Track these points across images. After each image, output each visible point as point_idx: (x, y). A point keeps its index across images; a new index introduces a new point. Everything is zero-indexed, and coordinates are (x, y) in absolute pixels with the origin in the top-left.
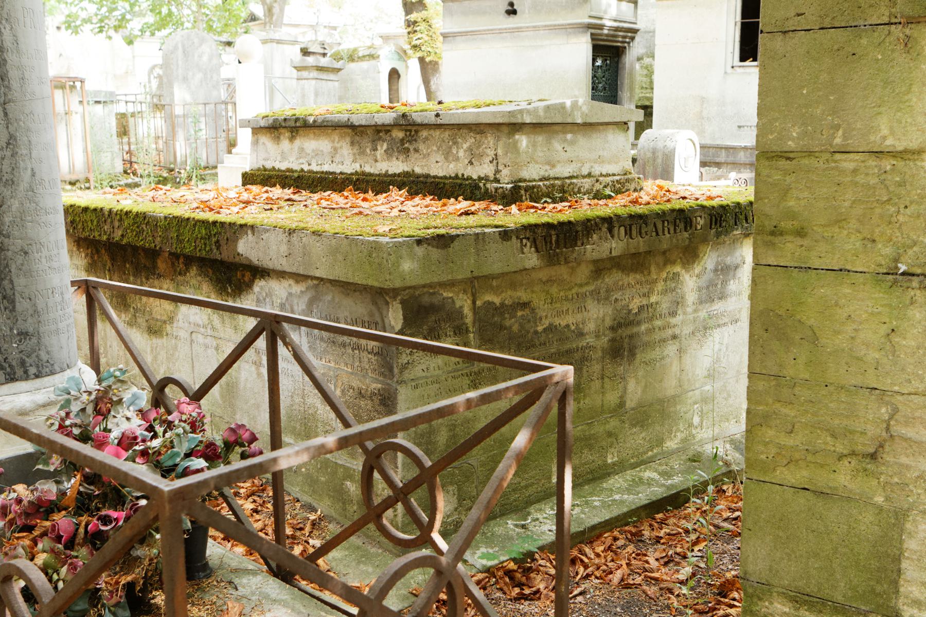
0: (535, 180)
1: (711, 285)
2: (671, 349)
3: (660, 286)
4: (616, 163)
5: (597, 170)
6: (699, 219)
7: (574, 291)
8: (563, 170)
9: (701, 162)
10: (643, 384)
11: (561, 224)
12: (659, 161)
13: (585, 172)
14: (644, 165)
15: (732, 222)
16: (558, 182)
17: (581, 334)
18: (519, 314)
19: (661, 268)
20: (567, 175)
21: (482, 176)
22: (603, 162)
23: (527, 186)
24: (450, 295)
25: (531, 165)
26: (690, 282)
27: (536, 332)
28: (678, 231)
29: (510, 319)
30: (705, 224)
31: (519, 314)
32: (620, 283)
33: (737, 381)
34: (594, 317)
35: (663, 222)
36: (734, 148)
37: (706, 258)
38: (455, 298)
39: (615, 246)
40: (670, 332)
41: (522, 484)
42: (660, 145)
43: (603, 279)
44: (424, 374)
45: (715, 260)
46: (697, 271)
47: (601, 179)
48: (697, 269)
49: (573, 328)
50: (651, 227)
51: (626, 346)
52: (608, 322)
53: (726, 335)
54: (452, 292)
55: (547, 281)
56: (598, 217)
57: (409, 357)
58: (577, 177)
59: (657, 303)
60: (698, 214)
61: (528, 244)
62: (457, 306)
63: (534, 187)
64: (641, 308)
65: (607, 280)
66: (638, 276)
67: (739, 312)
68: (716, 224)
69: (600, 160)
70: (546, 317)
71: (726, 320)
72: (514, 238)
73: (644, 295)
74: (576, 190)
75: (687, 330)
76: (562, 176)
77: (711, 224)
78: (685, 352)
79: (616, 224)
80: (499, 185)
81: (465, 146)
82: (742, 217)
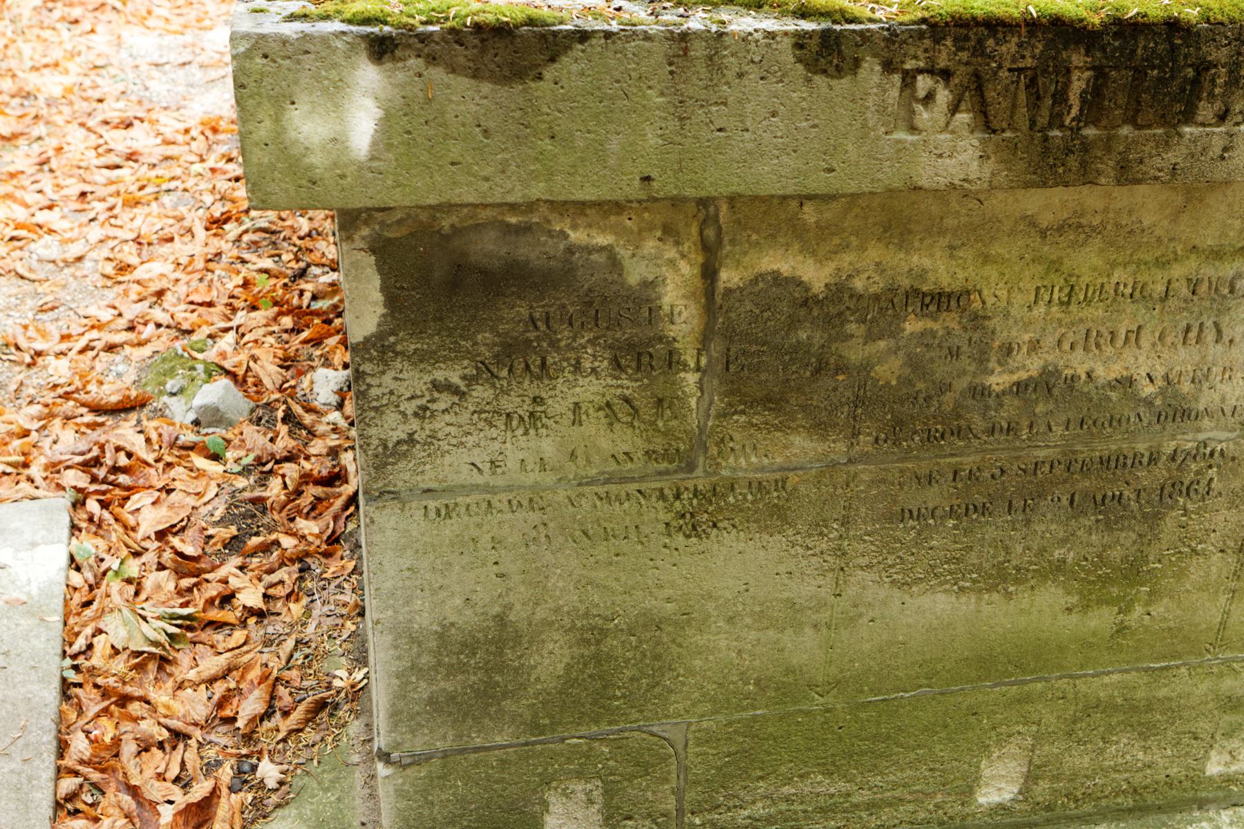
7: (1177, 271)
17: (1178, 412)
18: (912, 326)
24: (602, 240)
27: (979, 392)
29: (870, 338)
31: (912, 326)
38: (624, 253)
41: (855, 799)
44: (479, 480)
49: (1148, 390)
54: (618, 231)
55: (1061, 229)
57: (414, 424)
61: (943, 96)
62: (633, 279)
70: (1035, 346)
72: (871, 70)
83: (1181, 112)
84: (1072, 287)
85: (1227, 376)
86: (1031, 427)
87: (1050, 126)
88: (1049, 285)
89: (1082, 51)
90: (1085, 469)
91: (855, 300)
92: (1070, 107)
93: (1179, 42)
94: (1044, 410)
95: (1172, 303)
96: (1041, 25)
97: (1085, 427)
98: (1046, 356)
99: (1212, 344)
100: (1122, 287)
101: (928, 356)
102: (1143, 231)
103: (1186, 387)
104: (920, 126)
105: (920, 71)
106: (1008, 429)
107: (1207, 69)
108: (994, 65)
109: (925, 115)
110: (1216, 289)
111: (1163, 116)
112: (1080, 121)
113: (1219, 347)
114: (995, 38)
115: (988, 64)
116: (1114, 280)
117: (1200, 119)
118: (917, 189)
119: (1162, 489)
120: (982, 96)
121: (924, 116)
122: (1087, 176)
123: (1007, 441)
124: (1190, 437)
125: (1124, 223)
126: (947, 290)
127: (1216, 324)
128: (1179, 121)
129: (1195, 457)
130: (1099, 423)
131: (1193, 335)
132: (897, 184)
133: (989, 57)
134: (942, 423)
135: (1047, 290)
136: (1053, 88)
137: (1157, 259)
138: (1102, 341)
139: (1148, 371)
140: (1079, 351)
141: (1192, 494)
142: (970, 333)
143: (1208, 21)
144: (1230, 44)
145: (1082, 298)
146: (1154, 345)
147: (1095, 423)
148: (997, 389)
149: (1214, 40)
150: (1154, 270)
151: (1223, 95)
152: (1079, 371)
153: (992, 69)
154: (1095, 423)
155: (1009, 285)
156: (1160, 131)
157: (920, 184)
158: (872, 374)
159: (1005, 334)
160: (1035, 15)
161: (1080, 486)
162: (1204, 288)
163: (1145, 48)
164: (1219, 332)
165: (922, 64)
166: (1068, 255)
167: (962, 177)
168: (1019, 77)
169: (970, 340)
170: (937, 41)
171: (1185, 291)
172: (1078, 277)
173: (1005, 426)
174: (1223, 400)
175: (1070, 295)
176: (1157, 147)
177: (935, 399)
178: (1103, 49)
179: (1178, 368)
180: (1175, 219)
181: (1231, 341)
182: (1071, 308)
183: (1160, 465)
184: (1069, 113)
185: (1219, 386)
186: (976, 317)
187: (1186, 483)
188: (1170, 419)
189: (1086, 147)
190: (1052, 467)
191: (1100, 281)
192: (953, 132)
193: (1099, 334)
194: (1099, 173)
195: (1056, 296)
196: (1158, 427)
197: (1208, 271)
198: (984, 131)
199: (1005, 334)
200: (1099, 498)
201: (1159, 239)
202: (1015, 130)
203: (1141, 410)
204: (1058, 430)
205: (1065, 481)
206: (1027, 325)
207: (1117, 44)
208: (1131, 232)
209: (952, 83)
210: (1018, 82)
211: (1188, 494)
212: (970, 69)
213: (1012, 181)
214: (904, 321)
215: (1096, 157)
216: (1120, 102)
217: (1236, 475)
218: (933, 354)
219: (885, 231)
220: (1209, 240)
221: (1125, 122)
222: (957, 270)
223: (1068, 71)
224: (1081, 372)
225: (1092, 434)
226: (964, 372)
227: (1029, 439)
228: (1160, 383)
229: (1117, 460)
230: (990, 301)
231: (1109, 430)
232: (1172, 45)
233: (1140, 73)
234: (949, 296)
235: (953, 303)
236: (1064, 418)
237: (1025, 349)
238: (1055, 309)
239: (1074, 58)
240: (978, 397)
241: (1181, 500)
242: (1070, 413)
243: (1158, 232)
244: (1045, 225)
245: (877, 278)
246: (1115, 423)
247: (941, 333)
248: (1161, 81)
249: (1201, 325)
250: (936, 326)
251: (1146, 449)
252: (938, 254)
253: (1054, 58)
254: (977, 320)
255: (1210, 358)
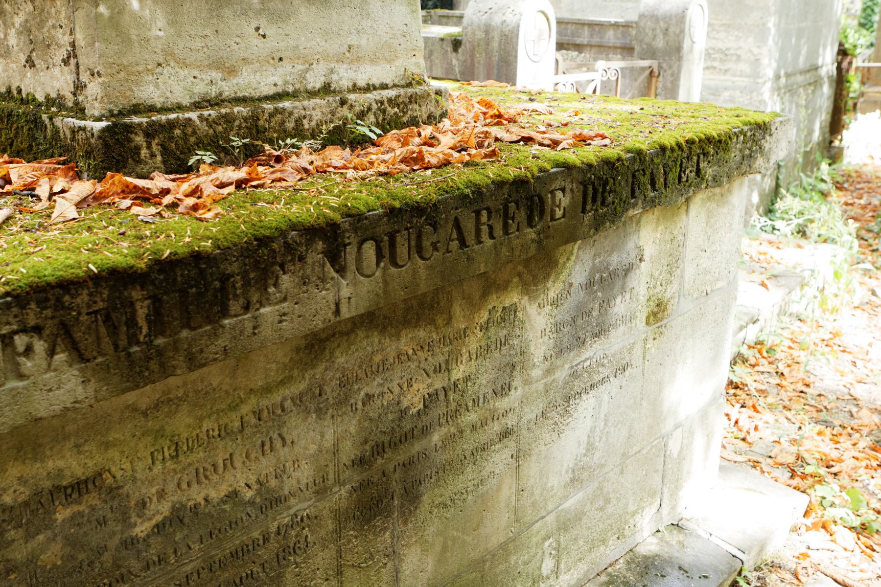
0: (179, 107)
1: (581, 312)
2: (499, 460)
3: (474, 342)
4: (389, 61)
5: (344, 77)
6: (559, 194)
7: (245, 409)
8: (262, 81)
9: (557, 44)
10: (438, 548)
11: (166, 267)
12: (495, 45)
13: (315, 81)
14: (473, 51)
15: (625, 193)
16: (241, 110)
17: (272, 501)
19: (473, 305)
20: (271, 91)
21: (53, 95)
22: (359, 59)
23: (152, 124)
25: (166, 71)
26: (538, 319)
27: (130, 543)
28: (513, 227)
29: (29, 536)
30: (573, 204)
32: (378, 358)
33: (622, 472)
34: (312, 448)
35: (478, 213)
36: (600, 25)
37: (570, 264)
39: (351, 291)
40: (496, 427)
42: (497, 20)
43: (331, 359)
45: (588, 265)
46: (552, 294)
47: (352, 97)
48: (554, 289)
49: (249, 494)
50: (449, 229)
51: (396, 487)
52: (349, 451)
53: (606, 398)
55: (157, 406)
56: (293, 226)
58: (294, 95)
59: (467, 379)
60: (557, 184)
61: (40, 346)
63: (171, 125)
64: (430, 400)
65: (341, 360)
66: (422, 333)
67: (630, 351)
68: (594, 201)
69: (352, 55)
71: (605, 372)
73: (438, 370)
74: (290, 125)
75: (530, 413)
76: (256, 94)
77: (585, 203)
78: (527, 454)
79: (351, 239)
80: (82, 123)
81: (18, 20)
82: (645, 180)
83: (218, 312)
84: (177, 444)
85: (296, 466)
86: (175, 552)
87: (130, 344)
88: (160, 448)
89: (138, 288)
90: (222, 565)
91: (7, 512)
92: (141, 328)
93: (204, 266)
94: (182, 536)
95: (248, 431)
96: (103, 277)
97: (214, 536)
98: (172, 498)
99: (281, 449)
100: (211, 432)
101: (81, 532)
102: (214, 390)
103: (273, 483)
104: (27, 372)
105: (16, 332)
106: (159, 561)
107: (228, 279)
108: (74, 313)
109: (29, 364)
110: (273, 412)
111: (208, 317)
112: (150, 336)
113: (286, 449)
114: (69, 294)
115: (70, 314)
116: (204, 429)
117: (233, 313)
118: (38, 420)
119: (278, 556)
120: (71, 337)
121: (27, 365)
122: (166, 371)
123: (161, 569)
124: (285, 514)
125: (200, 388)
126: (83, 478)
127: (280, 435)
128: (219, 318)
129: (292, 526)
130: (223, 530)
131: (267, 447)
132: (20, 421)
133: (69, 309)
134: (107, 577)
135: (159, 452)
136: (124, 318)
137: (229, 405)
138: (208, 473)
139: (245, 481)
140: (195, 486)
141: (298, 551)
142: (110, 503)
143: (219, 248)
144: (238, 260)
145: (185, 448)
146: (244, 463)
147: (220, 531)
148: (142, 535)
149: (227, 260)
150: (230, 414)
151: (243, 293)
152: (198, 500)
153: (73, 317)
154: (220, 531)
155: (130, 458)
156: (208, 328)
157: (39, 415)
158: (39, 563)
159: (137, 494)
160: (96, 271)
161: (222, 579)
162: (265, 415)
163: (182, 275)
164: (283, 439)
165: (15, 327)
166: (167, 423)
167: (72, 400)
168: (96, 317)
169: (111, 508)
170: (23, 307)
171: (254, 421)
172: (179, 435)
173: (156, 559)
174: (299, 482)
175: (177, 450)
176: (210, 339)
177: (97, 561)
178: (153, 283)
179: (264, 472)
180: (233, 375)
181: (292, 442)
182: (180, 459)
183: (271, 541)
184: (141, 333)
185: (293, 474)
186: (111, 490)
187: (292, 545)
188: (269, 507)
189: (160, 352)
190: (198, 574)
191: (195, 433)
192: (55, 370)
193: (205, 469)
194: (175, 367)
195: (167, 454)
196: (263, 517)
197: (265, 402)
198: (80, 362)
199: (137, 494)
200: (238, 581)
201: (227, 392)
202: (104, 355)
203: (249, 510)
204: (196, 547)
205: (211, 580)
206: (151, 482)
207: (162, 277)
208: (207, 393)
209: (44, 335)
210: (96, 321)
211: (295, 552)
212: (56, 321)
213: (112, 392)
214: (55, 513)
215: (170, 357)
216: (176, 315)
217: (320, 526)
218: (85, 529)
219: (19, 451)
220: (259, 382)
221: (183, 327)
222: (86, 461)
223: (132, 304)
224: (200, 499)
225: (220, 540)
226: (114, 533)
227: (176, 561)
228: (255, 487)
229: (243, 550)
230: (119, 474)
231: (231, 532)
232: (200, 269)
233: (183, 292)
234: (86, 482)
235: (90, 486)
236: (197, 536)
237: (155, 499)
238: (168, 464)
239: (134, 294)
240: (130, 547)
241: (292, 558)
242: (200, 532)
243: (225, 388)
244: (144, 407)
245: (22, 489)
246: (233, 526)
247: (87, 511)
248: (199, 294)
249: (271, 438)
250: (81, 508)
251: (260, 534)
252: (68, 454)
253: (119, 298)
254: (113, 491)
255: (283, 458)
